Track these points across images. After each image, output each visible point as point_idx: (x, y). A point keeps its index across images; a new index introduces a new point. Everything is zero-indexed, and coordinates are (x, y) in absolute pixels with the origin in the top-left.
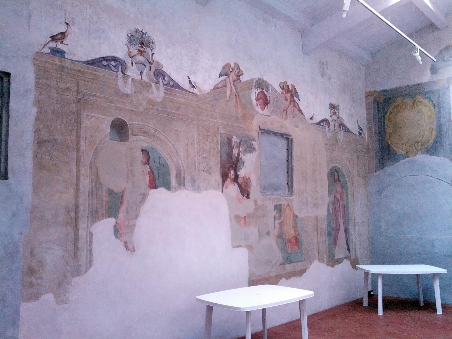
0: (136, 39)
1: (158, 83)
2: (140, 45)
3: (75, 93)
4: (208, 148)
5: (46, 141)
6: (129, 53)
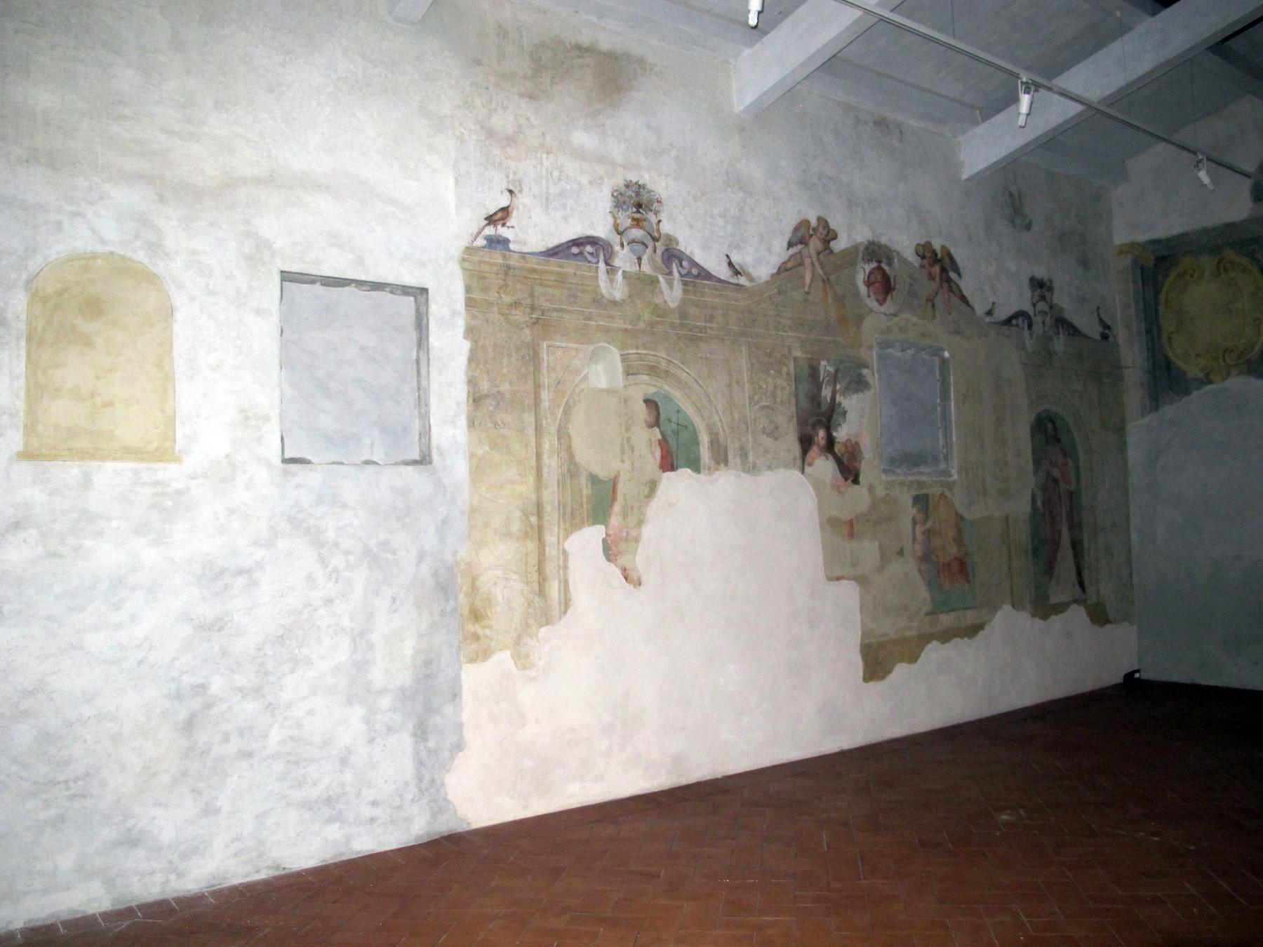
1: (670, 273)
3: (528, 310)
4: (770, 388)
5: (486, 396)
6: (616, 226)
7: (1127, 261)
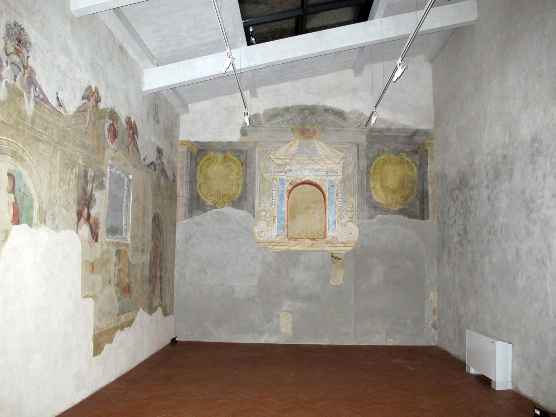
0: (14, 34)
1: (29, 93)
2: (17, 43)
6: (6, 49)
7: (185, 148)
